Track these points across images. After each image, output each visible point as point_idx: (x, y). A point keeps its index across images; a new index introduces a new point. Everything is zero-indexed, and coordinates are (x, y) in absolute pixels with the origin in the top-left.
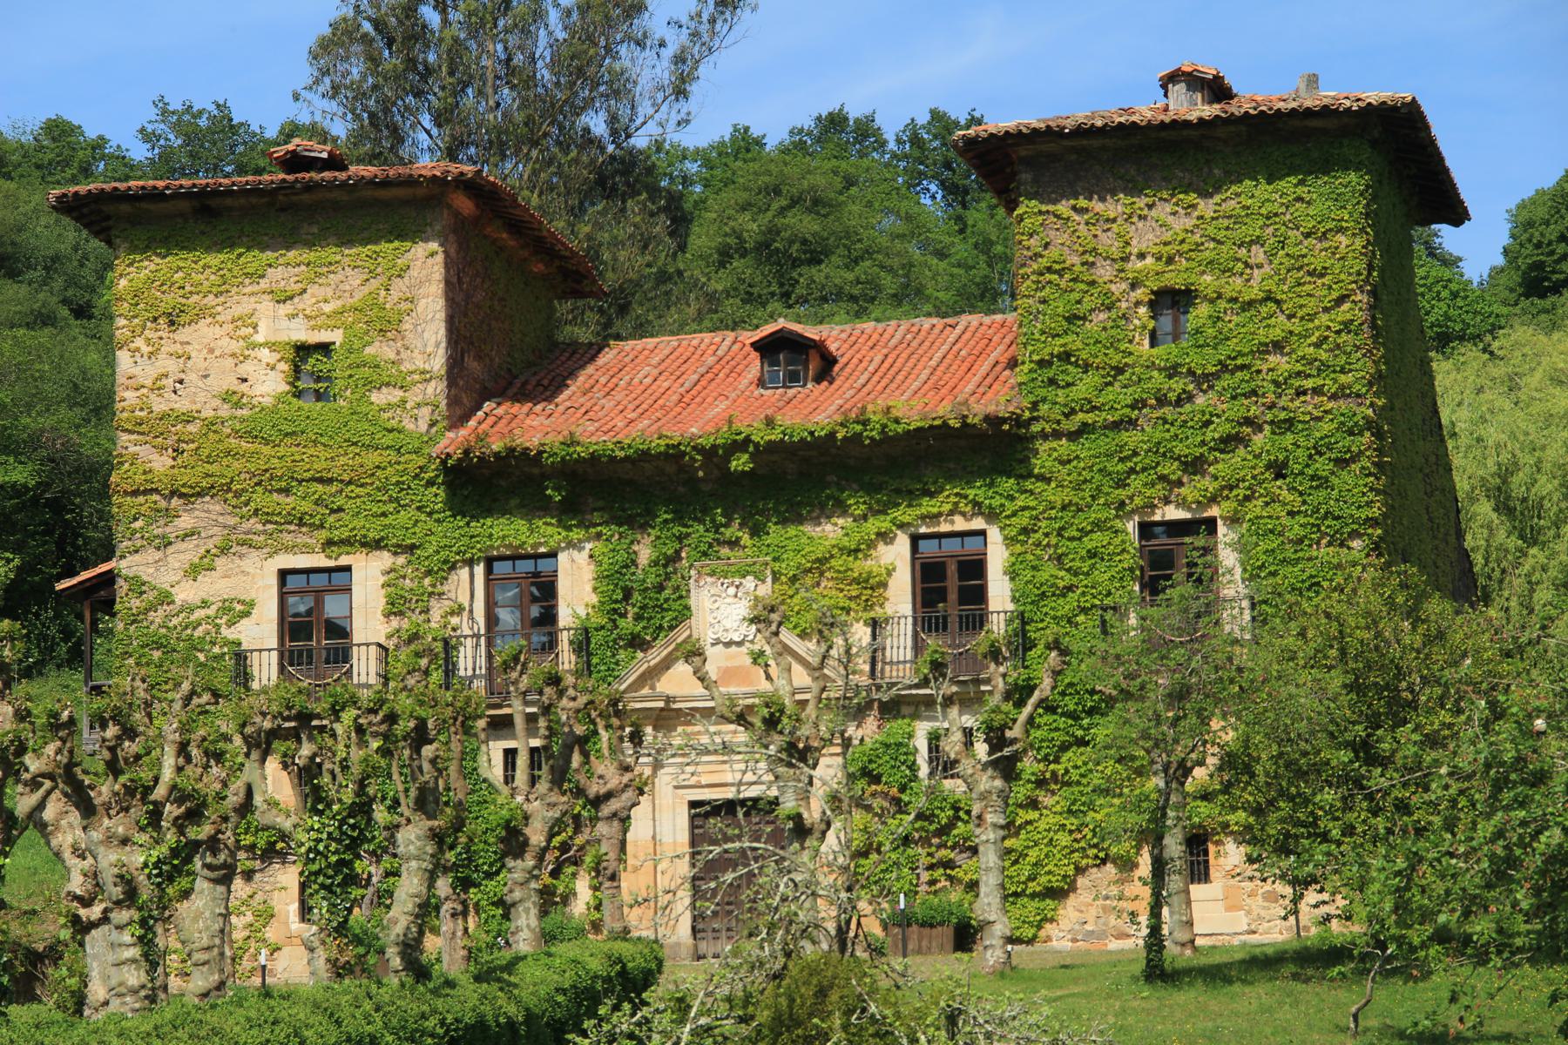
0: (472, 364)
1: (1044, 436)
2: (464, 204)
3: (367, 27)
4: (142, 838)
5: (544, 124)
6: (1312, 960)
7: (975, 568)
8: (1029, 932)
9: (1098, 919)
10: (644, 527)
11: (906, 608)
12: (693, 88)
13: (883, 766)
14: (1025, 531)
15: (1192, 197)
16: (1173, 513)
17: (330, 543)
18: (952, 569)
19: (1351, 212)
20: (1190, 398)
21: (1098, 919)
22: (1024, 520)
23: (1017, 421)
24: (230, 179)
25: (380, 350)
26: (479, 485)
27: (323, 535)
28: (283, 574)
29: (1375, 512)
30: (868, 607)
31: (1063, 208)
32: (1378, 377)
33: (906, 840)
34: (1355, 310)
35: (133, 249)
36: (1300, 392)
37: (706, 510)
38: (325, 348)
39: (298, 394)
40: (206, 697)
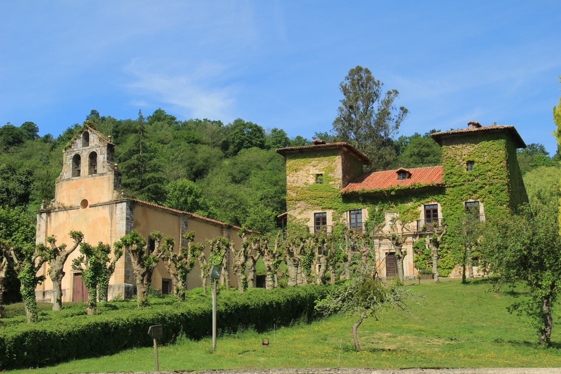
0: (347, 177)
1: (448, 187)
2: (345, 149)
3: (342, 119)
4: (272, 260)
5: (373, 134)
6: (485, 281)
7: (436, 211)
8: (446, 275)
9: (455, 274)
10: (377, 204)
11: (424, 218)
12: (399, 127)
13: (419, 246)
14: (444, 204)
15: (473, 144)
16: (471, 200)
17: (323, 208)
18: (432, 211)
19: (503, 146)
20: (474, 180)
21: (455, 274)
22: (444, 202)
23: (443, 185)
24: (306, 146)
25: (331, 175)
26: (348, 198)
27: (321, 207)
28: (315, 214)
29: (508, 200)
30: (417, 218)
31: (450, 147)
32: (508, 176)
33: (424, 259)
34: (504, 164)
35: (289, 159)
36: (494, 179)
37: (388, 201)
38: (321, 175)
39: (317, 183)
40: (189, 244)
